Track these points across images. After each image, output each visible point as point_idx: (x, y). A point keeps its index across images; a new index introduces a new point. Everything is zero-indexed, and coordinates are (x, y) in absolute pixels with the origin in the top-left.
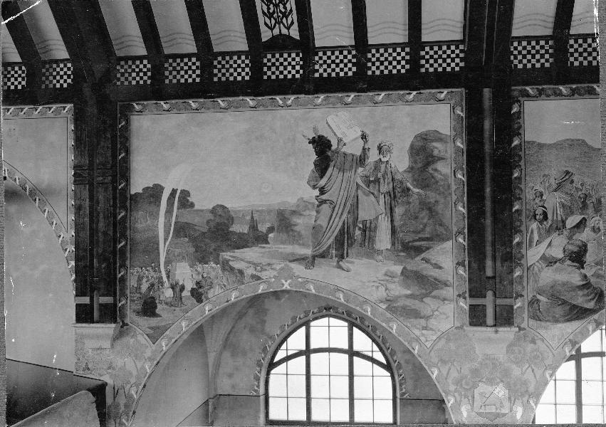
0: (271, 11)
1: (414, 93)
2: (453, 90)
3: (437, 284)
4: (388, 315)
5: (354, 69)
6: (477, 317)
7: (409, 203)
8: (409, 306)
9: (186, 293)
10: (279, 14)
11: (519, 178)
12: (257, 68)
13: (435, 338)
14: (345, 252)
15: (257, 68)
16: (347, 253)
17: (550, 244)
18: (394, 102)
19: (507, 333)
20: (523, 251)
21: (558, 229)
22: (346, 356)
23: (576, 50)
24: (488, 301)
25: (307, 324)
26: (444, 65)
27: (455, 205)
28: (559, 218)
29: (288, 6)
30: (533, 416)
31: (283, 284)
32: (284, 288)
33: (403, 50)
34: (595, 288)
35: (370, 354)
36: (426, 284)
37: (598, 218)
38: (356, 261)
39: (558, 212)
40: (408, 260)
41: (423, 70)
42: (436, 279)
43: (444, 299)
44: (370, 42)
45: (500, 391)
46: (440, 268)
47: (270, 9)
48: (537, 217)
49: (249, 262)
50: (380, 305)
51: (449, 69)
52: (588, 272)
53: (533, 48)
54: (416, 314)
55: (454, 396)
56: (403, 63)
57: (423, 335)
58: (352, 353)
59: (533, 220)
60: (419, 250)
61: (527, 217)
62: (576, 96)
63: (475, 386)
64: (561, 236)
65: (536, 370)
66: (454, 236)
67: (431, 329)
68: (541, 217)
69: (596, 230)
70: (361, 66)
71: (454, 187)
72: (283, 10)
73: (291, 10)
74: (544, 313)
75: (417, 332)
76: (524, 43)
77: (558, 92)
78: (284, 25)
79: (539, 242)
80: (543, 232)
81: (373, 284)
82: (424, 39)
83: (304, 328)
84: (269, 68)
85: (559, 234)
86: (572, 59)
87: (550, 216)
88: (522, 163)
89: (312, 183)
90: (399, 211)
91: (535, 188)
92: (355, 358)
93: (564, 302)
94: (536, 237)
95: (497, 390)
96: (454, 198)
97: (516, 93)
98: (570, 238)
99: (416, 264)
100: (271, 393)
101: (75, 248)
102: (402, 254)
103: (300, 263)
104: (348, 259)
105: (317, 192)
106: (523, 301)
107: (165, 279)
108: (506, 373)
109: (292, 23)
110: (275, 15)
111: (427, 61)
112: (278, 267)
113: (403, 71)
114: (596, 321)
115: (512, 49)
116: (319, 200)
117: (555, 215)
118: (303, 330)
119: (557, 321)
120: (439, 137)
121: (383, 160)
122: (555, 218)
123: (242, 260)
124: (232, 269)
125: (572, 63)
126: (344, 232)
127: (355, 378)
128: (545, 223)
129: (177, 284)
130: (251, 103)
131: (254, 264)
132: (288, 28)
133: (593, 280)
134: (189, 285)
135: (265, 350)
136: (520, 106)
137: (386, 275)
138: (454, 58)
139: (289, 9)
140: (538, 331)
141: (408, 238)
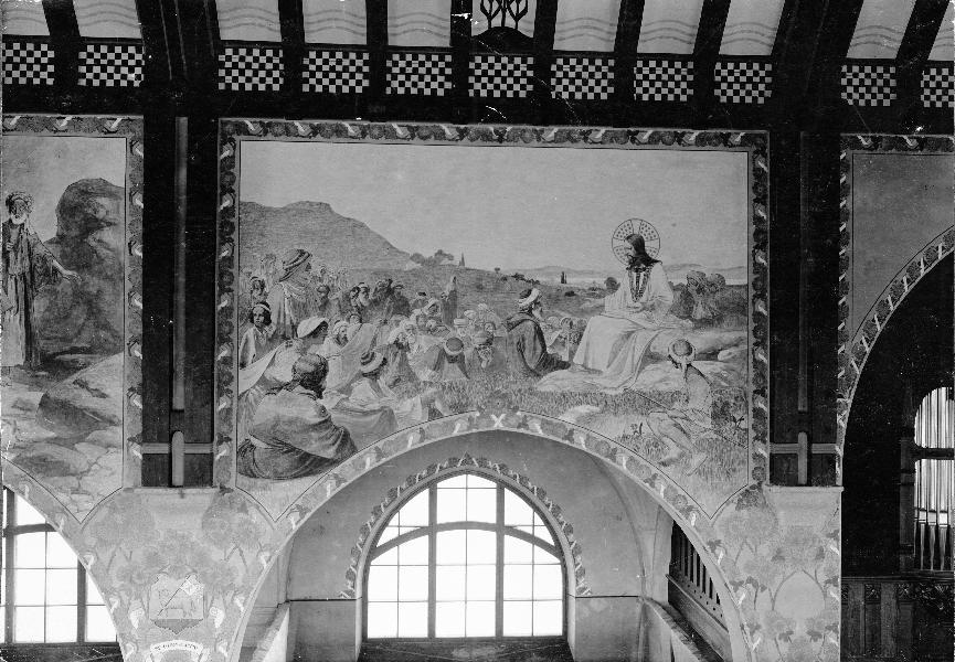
1: (69, 117)
2: (131, 117)
3: (98, 420)
5: (366, 83)
6: (156, 473)
7: (55, 293)
11: (230, 259)
12: (460, 75)
15: (460, 75)
17: (272, 362)
18: (36, 130)
19: (201, 497)
21: (284, 337)
22: (493, 535)
23: (646, 77)
24: (180, 447)
25: (432, 486)
26: (665, 91)
27: (130, 297)
28: (288, 323)
31: (494, 422)
32: (495, 427)
34: (337, 428)
35: (529, 530)
36: (79, 421)
37: (345, 322)
40: (52, 383)
42: (94, 413)
44: (392, 42)
45: (192, 588)
46: (103, 396)
51: (671, 98)
52: (328, 402)
53: (242, 59)
54: (64, 470)
55: (120, 597)
56: (762, 87)
57: (73, 502)
58: (501, 529)
59: (249, 323)
60: (71, 368)
61: (240, 317)
62: (270, 136)
63: (152, 580)
65: (245, 552)
66: (126, 346)
68: (262, 318)
70: (378, 73)
71: (128, 271)
74: (260, 465)
75: (63, 497)
77: (292, 129)
78: (511, 12)
79: (256, 358)
80: (263, 342)
82: (309, 39)
83: (427, 491)
86: (639, 90)
87: (273, 318)
88: (234, 236)
90: (39, 305)
91: (252, 275)
92: (508, 539)
93: (292, 449)
94: (252, 350)
95: (186, 585)
96: (129, 286)
97: (229, 128)
98: (303, 351)
99: (65, 390)
100: (370, 597)
101: (143, 352)
102: (43, 373)
108: (202, 559)
113: (604, 96)
114: (336, 476)
117: (282, 317)
118: (425, 493)
119: (280, 478)
120: (104, 189)
121: (14, 222)
122: (282, 321)
125: (640, 96)
127: (438, 568)
128: (267, 328)
132: (517, 18)
133: (334, 416)
135: (365, 530)
136: (234, 148)
138: (46, 64)
140: (253, 493)
141: (53, 348)
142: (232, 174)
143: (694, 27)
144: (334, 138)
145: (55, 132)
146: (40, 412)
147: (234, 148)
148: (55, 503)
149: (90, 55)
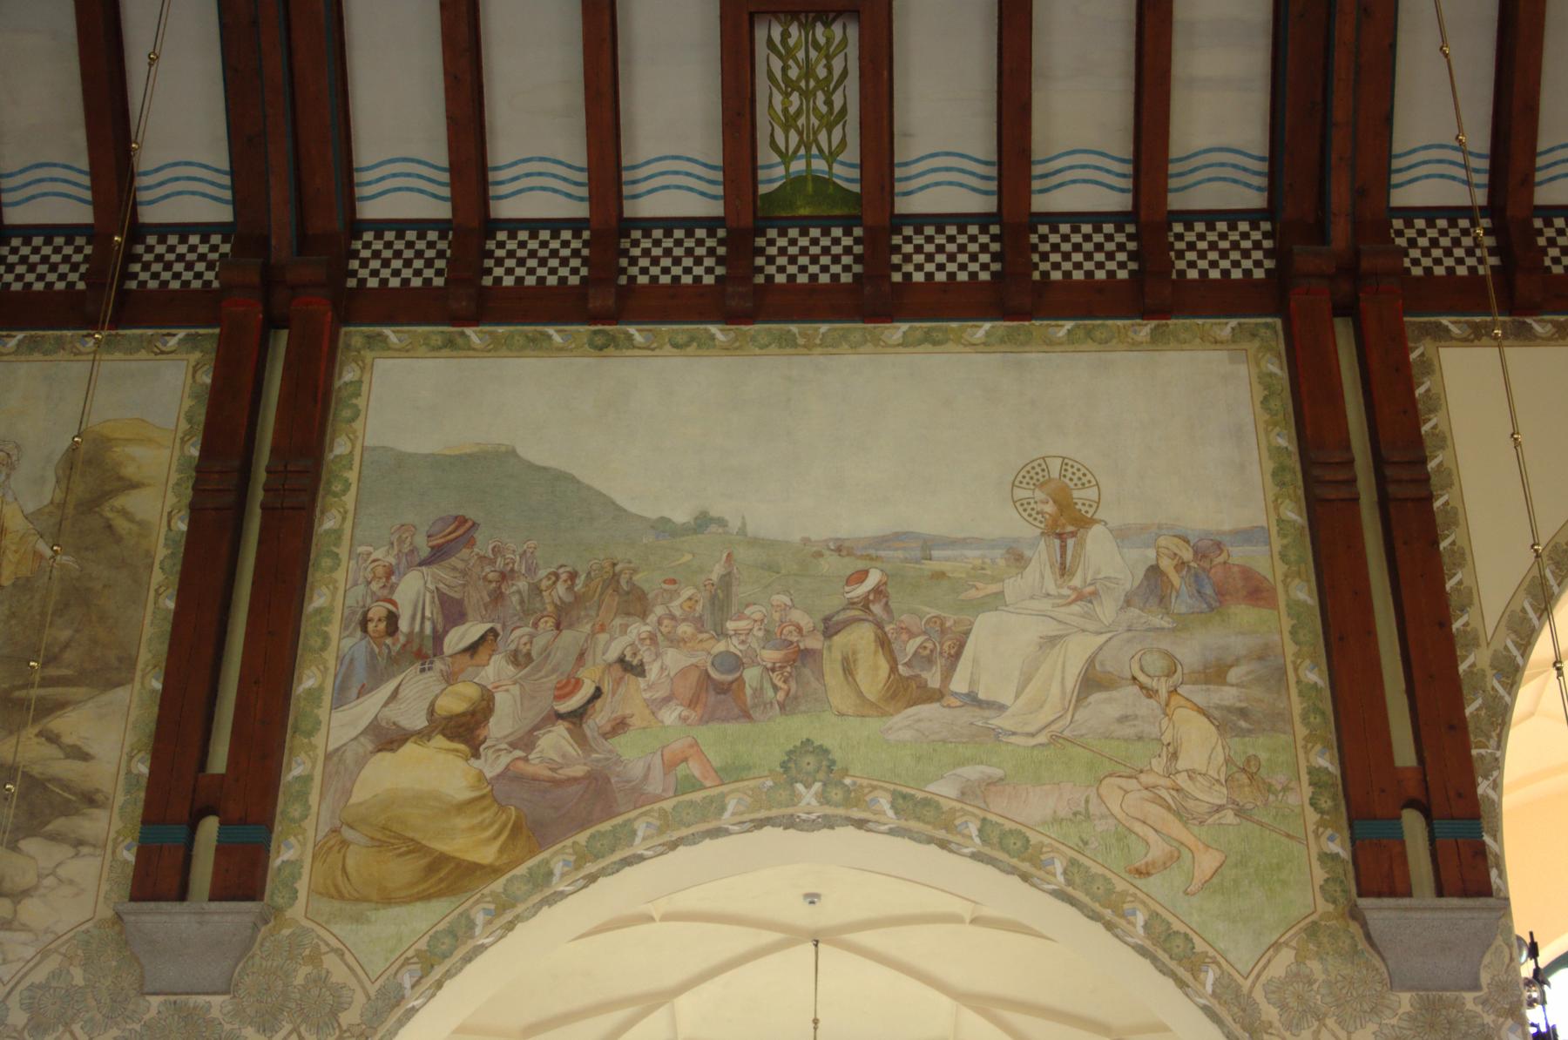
0: (792, 110)
13: (29, 952)
17: (395, 695)
20: (323, 713)
21: (420, 656)
33: (1120, 229)
39: (428, 614)
41: (897, 277)
43: (79, 843)
46: (85, 757)
48: (371, 626)
64: (429, 674)
68: (382, 626)
69: (519, 659)
73: (844, 110)
84: (1044, 257)
85: (423, 670)
87: (403, 625)
91: (372, 557)
110: (801, 121)
111: (146, 267)
115: (1171, 239)
132: (831, 157)
139: (837, 106)
143: (1261, 159)
144: (445, 352)
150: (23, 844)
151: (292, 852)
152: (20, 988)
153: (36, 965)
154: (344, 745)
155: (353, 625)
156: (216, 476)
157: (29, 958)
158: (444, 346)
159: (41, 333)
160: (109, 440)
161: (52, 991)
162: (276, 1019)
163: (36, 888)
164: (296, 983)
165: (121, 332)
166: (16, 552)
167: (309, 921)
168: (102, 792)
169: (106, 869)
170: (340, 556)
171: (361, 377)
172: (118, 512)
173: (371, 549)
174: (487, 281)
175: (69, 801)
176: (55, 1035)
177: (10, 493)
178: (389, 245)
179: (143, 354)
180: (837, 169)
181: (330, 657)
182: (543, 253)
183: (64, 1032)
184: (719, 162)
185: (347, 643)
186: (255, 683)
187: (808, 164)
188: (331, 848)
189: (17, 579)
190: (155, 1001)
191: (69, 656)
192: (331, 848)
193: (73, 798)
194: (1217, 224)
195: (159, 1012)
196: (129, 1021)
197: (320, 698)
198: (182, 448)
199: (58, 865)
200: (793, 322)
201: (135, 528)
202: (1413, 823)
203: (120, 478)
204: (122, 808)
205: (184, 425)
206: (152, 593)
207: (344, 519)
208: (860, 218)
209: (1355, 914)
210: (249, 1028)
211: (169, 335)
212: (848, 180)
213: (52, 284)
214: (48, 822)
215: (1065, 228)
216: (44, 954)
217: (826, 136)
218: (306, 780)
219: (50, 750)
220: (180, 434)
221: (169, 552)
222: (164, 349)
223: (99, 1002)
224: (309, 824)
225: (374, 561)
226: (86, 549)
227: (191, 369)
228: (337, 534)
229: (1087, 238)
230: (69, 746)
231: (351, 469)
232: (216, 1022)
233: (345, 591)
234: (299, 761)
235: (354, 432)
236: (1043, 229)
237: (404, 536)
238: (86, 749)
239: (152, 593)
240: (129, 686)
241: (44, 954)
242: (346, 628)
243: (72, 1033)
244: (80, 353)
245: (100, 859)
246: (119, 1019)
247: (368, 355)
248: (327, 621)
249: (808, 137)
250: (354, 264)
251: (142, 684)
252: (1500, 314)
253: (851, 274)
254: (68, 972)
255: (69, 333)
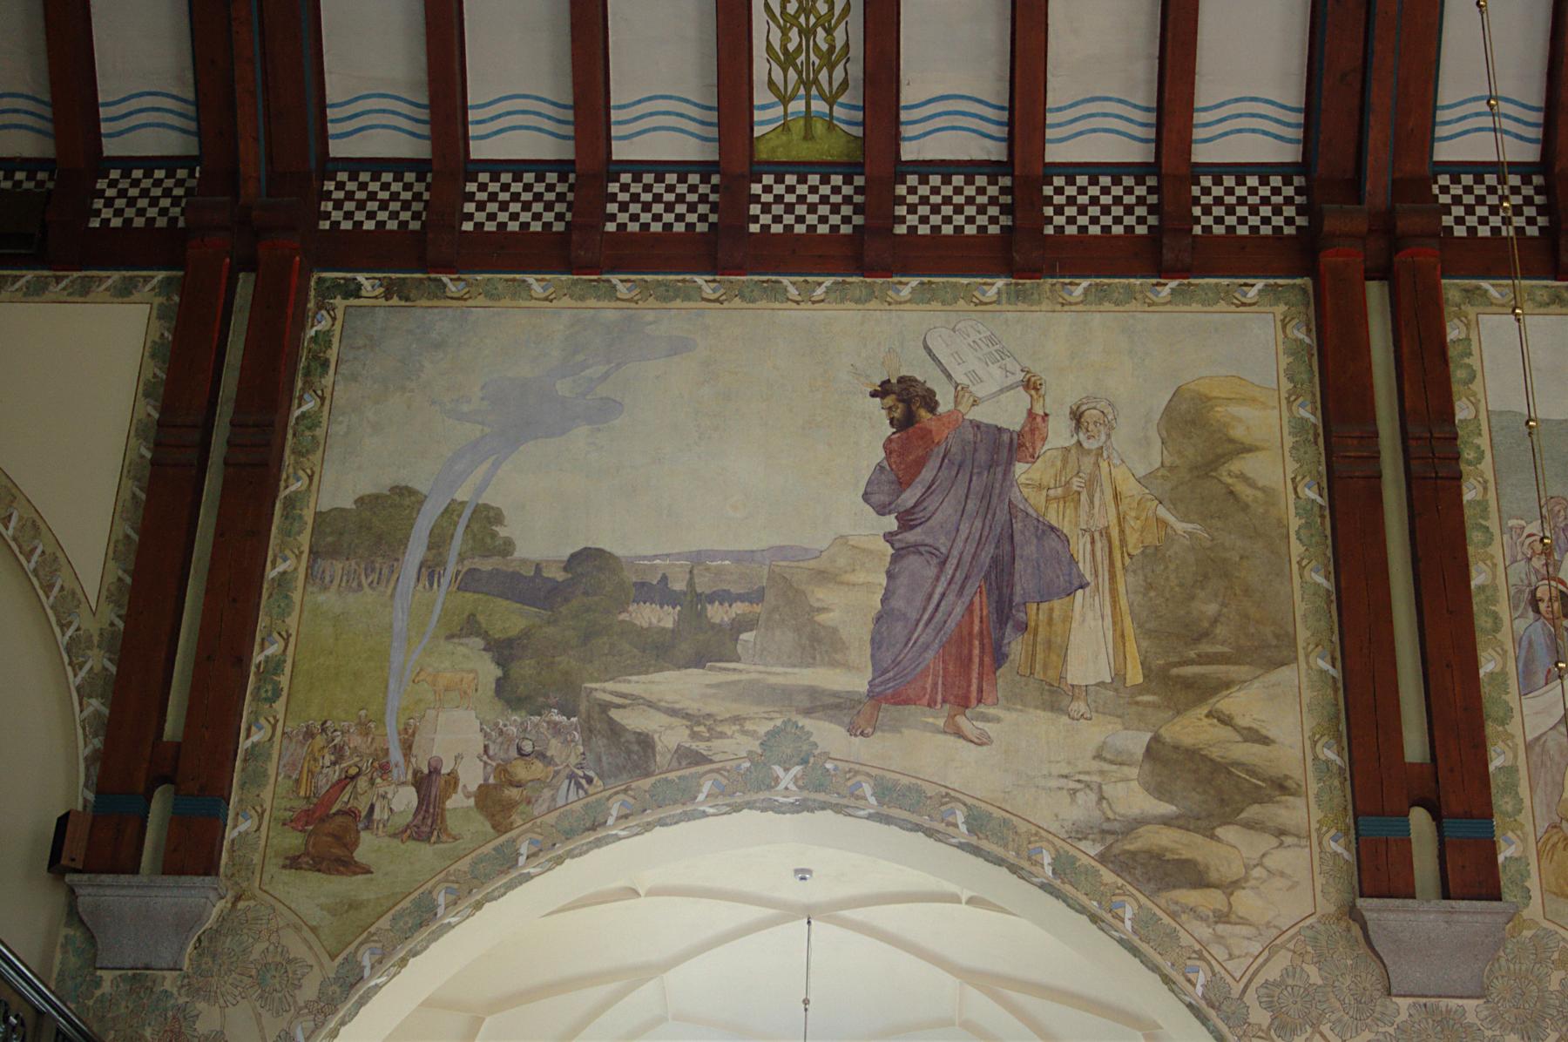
0: (791, 47)
4: (1108, 876)
8: (1172, 851)
9: (457, 802)
10: (813, 57)
13: (1256, 947)
14: (974, 687)
16: (980, 690)
20: (1512, 697)
29: (839, 34)
30: (893, 436)
33: (1287, 181)
38: (1009, 717)
43: (1281, 833)
46: (1265, 741)
47: (790, 40)
49: (673, 712)
50: (1082, 845)
54: (1194, 875)
56: (1141, 211)
57: (1219, 939)
67: (1243, 921)
72: (824, 47)
76: (671, 178)
81: (1063, 782)
89: (879, 498)
103: (831, 719)
104: (982, 708)
105: (891, 523)
106: (1524, 840)
107: (396, 755)
109: (845, 84)
112: (764, 728)
116: (897, 545)
121: (1086, 445)
123: (651, 705)
124: (615, 730)
126: (970, 634)
129: (434, 771)
130: (708, 291)
131: (687, 716)
134: (472, 776)
137: (1098, 756)
139: (839, 44)
142: (1469, 366)
143: (1147, 109)
144: (1554, 308)
145: (1063, 305)
146: (1147, 767)
147: (1468, 326)
148: (1185, 939)
149: (768, 189)
150: (1219, 831)
151: (1513, 848)
152: (1253, 986)
153: (1266, 961)
154: (1545, 733)
155: (1522, 605)
156: (1355, 442)
157: (1257, 953)
158: (1552, 302)
159: (1106, 281)
160: (1210, 399)
161: (1289, 989)
162: (1539, 1026)
163: (1246, 879)
164: (1551, 989)
165: (1193, 281)
166: (1137, 518)
167: (1547, 922)
168: (1291, 778)
169: (1316, 863)
170: (1491, 530)
171: (1468, 335)
172: (1237, 477)
173: (1523, 523)
174: (95, 223)
175: (1257, 787)
176: (1304, 1037)
177: (1115, 454)
178: (528, 188)
179: (1222, 306)
180: (838, 111)
181: (1505, 635)
182: (647, 197)
183: (1313, 1033)
184: (569, 101)
185: (1520, 625)
186: (1447, 666)
187: (808, 105)
188: (1554, 846)
189: (1145, 547)
190: (1404, 1003)
191: (1220, 630)
192: (1554, 846)
193: (1263, 785)
194: (1271, 178)
195: (1410, 1015)
196: (1379, 1023)
197: (1505, 682)
198: (1290, 410)
199: (1263, 855)
200: (1135, 277)
201: (1259, 494)
202: (1419, 819)
203: (1231, 441)
204: (1317, 796)
205: (1286, 385)
206: (1295, 567)
207: (1485, 489)
208: (862, 165)
209: (1354, 914)
210: (1512, 1035)
211: (1246, 285)
212: (849, 123)
213: (131, 220)
214: (1242, 810)
215: (1082, 180)
216: (1272, 949)
217: (827, 75)
218: (1511, 770)
219: (1225, 732)
220: (1284, 395)
221: (1303, 521)
222: (1244, 300)
223: (1342, 1002)
224: (1525, 818)
225: (1529, 536)
226: (1212, 517)
227: (1279, 324)
228: (1482, 505)
229: (1468, 190)
230: (1245, 728)
231: (1480, 435)
232: (1475, 1028)
233: (1506, 568)
234: (1499, 750)
235: (1474, 395)
236: (1206, 181)
237: (1557, 508)
238: (1264, 732)
239: (1295, 567)
240: (1295, 666)
241: (1272, 949)
242: (1516, 607)
243: (1322, 1035)
244: (1152, 304)
245: (1307, 850)
246: (1369, 1021)
247: (1471, 311)
248: (1495, 602)
249: (808, 74)
250: (98, 204)
251: (1308, 663)
252: (1524, 277)
253: (851, 226)
254: (1302, 970)
255: (1138, 282)
